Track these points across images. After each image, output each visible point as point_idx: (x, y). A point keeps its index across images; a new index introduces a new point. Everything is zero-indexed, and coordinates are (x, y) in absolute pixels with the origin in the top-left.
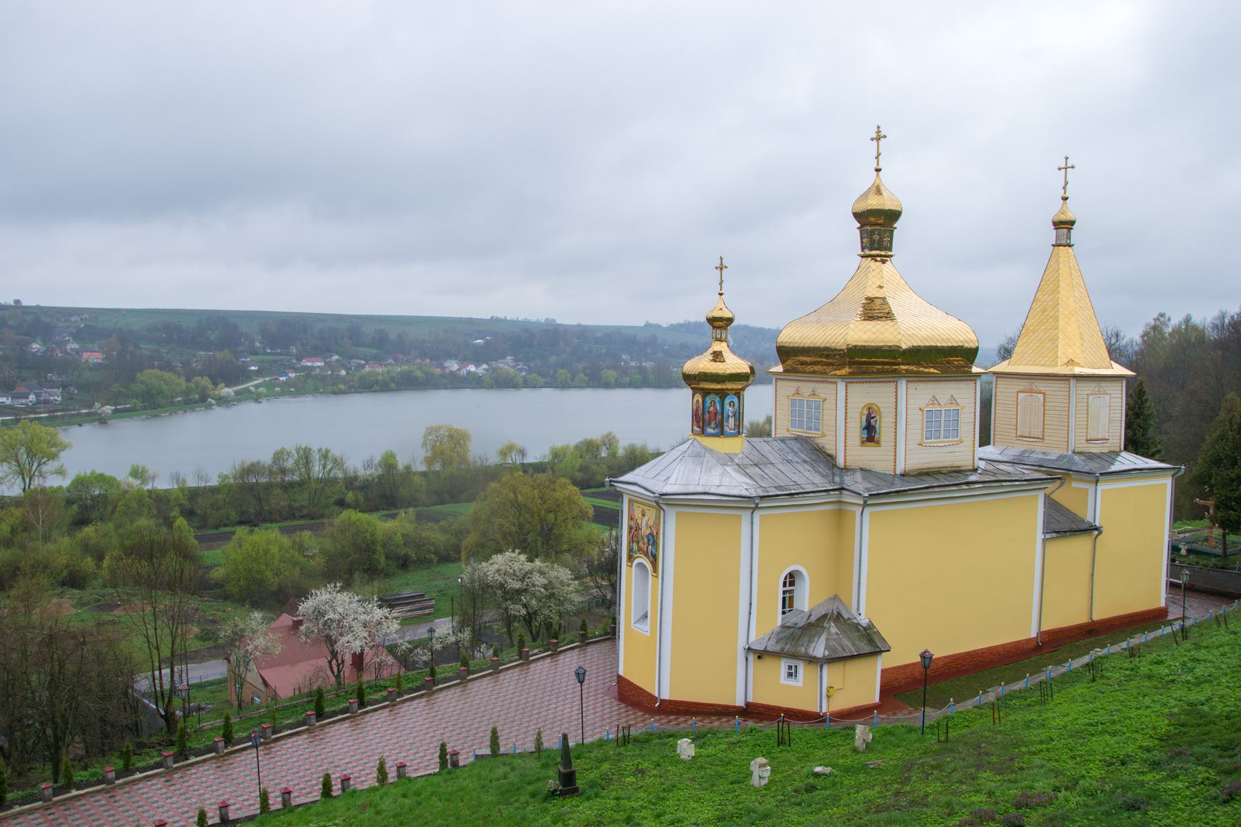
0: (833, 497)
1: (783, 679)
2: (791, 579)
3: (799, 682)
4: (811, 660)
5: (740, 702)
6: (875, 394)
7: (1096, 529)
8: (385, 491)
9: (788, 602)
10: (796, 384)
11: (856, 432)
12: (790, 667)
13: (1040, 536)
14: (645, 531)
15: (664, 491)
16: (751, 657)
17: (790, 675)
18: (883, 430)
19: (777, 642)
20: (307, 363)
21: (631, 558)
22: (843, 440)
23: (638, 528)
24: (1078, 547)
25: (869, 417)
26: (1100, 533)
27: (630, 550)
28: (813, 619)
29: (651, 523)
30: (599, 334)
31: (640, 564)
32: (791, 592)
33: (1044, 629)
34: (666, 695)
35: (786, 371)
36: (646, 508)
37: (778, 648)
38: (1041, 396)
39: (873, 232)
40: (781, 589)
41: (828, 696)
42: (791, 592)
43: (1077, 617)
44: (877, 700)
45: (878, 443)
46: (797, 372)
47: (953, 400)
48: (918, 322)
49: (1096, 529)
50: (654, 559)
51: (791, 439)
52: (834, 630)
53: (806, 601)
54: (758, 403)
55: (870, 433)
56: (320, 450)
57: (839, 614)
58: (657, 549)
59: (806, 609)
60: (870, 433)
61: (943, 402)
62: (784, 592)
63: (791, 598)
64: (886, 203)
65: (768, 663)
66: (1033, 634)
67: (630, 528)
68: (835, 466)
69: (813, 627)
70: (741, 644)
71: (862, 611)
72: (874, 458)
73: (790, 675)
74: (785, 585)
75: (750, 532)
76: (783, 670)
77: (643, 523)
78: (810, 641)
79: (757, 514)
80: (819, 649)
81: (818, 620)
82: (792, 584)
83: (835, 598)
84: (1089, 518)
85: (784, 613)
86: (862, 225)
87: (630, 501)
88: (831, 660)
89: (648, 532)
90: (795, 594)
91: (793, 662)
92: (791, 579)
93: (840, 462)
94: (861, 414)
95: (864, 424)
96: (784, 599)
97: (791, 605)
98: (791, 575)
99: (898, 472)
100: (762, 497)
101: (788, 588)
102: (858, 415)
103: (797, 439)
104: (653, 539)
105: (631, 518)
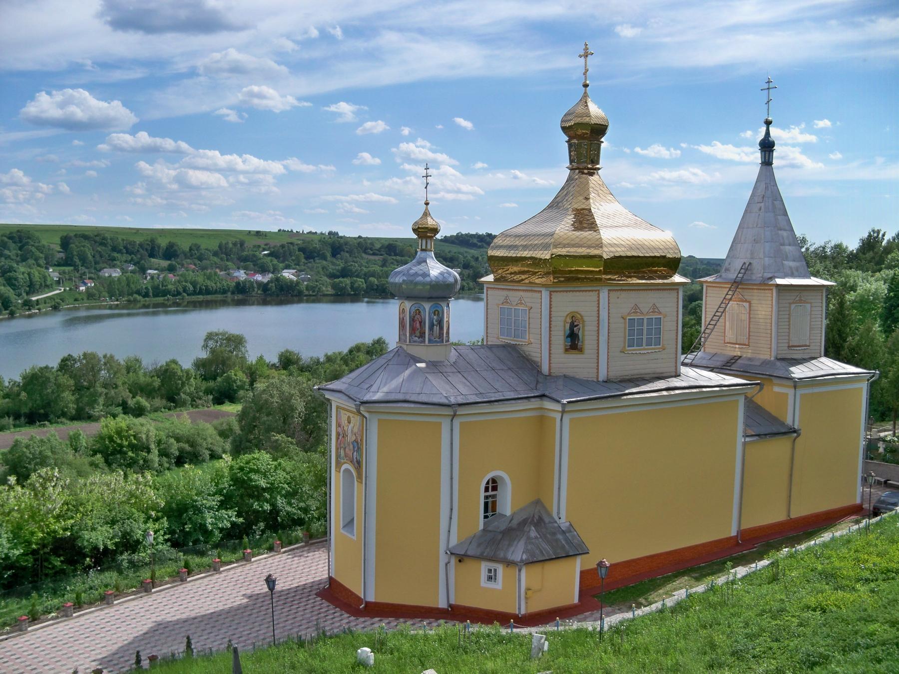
0: (535, 404)
1: (484, 583)
2: (493, 485)
3: (498, 585)
4: (509, 563)
5: (442, 604)
6: (573, 302)
7: (795, 431)
8: (168, 388)
9: (490, 507)
10: (505, 293)
11: (560, 340)
12: (490, 571)
13: (740, 440)
14: (351, 438)
15: (367, 398)
16: (453, 560)
17: (490, 578)
18: (586, 338)
19: (479, 545)
20: (106, 273)
21: (339, 465)
22: (544, 347)
23: (345, 435)
24: (779, 448)
25: (573, 326)
26: (799, 435)
27: (338, 456)
28: (515, 522)
29: (356, 430)
30: (138, 240)
31: (347, 470)
32: (494, 496)
33: (743, 527)
34: (371, 598)
35: (496, 280)
36: (351, 415)
37: (478, 552)
38: (746, 305)
39: (579, 145)
40: (482, 494)
41: (526, 598)
42: (494, 496)
43: (774, 515)
44: (576, 600)
45: (581, 350)
46: (506, 281)
47: (655, 309)
48: (619, 229)
49: (795, 431)
50: (358, 465)
51: (498, 346)
52: (533, 533)
53: (507, 505)
54: (466, 320)
55: (573, 341)
56: (105, 356)
57: (541, 519)
58: (361, 456)
59: (508, 513)
60: (573, 341)
61: (645, 310)
62: (486, 497)
63: (494, 504)
64: (430, 222)
65: (470, 565)
66: (733, 533)
67: (338, 434)
68: (539, 372)
69: (513, 532)
70: (442, 547)
71: (563, 514)
72: (574, 365)
73: (490, 578)
74: (487, 489)
75: (449, 436)
76: (484, 574)
77: (349, 429)
78: (510, 545)
79: (602, 376)
80: (518, 553)
81: (519, 524)
82: (495, 488)
83: (538, 502)
84: (789, 421)
85: (486, 517)
86: (571, 138)
87: (338, 407)
88: (528, 563)
89: (354, 438)
90: (498, 499)
91: (492, 565)
92: (493, 485)
93: (545, 369)
94: (565, 321)
95: (568, 332)
96: (486, 504)
97: (494, 510)
98: (494, 481)
99: (601, 379)
100: (460, 405)
101: (490, 493)
102: (562, 324)
103: (505, 347)
104: (358, 446)
105: (339, 425)
